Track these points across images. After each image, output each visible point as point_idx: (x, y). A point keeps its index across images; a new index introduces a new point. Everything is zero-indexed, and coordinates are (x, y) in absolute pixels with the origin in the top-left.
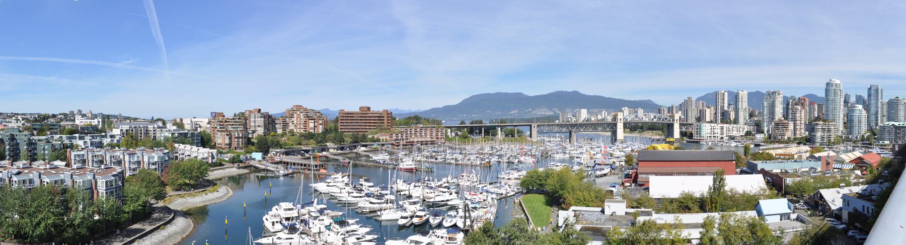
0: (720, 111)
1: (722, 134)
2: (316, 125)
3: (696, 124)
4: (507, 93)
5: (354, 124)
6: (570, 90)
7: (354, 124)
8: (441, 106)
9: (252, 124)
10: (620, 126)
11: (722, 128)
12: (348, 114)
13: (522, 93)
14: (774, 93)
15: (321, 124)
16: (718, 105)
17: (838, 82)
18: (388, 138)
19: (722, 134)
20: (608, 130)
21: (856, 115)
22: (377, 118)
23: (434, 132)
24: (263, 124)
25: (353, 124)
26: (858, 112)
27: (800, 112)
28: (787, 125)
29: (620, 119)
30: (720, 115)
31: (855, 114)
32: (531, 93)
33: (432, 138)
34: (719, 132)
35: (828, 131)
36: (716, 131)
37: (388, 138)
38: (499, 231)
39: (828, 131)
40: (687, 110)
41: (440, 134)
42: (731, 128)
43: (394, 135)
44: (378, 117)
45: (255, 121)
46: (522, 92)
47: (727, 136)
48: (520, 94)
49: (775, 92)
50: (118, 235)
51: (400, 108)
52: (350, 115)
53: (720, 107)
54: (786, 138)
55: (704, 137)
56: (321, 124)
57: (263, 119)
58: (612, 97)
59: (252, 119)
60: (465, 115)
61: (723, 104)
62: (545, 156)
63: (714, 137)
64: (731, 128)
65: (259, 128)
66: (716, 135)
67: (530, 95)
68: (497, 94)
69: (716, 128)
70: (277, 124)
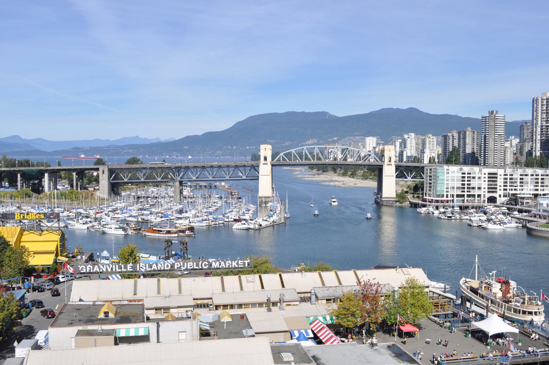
0: (539, 137)
1: (492, 189)
3: (428, 168)
4: (303, 113)
6: (404, 106)
8: (200, 134)
10: (389, 172)
11: (493, 177)
13: (327, 113)
16: (536, 124)
19: (492, 189)
27: (460, 146)
29: (265, 159)
30: (539, 145)
32: (340, 112)
34: (485, 185)
36: (475, 183)
38: (344, 355)
40: (485, 137)
42: (517, 176)
47: (504, 196)
48: (324, 114)
50: (517, 286)
51: (142, 136)
53: (539, 130)
55: (443, 196)
58: (459, 115)
60: (235, 147)
62: (317, 219)
63: (469, 196)
64: (517, 176)
66: (476, 192)
68: (288, 114)
69: (477, 176)
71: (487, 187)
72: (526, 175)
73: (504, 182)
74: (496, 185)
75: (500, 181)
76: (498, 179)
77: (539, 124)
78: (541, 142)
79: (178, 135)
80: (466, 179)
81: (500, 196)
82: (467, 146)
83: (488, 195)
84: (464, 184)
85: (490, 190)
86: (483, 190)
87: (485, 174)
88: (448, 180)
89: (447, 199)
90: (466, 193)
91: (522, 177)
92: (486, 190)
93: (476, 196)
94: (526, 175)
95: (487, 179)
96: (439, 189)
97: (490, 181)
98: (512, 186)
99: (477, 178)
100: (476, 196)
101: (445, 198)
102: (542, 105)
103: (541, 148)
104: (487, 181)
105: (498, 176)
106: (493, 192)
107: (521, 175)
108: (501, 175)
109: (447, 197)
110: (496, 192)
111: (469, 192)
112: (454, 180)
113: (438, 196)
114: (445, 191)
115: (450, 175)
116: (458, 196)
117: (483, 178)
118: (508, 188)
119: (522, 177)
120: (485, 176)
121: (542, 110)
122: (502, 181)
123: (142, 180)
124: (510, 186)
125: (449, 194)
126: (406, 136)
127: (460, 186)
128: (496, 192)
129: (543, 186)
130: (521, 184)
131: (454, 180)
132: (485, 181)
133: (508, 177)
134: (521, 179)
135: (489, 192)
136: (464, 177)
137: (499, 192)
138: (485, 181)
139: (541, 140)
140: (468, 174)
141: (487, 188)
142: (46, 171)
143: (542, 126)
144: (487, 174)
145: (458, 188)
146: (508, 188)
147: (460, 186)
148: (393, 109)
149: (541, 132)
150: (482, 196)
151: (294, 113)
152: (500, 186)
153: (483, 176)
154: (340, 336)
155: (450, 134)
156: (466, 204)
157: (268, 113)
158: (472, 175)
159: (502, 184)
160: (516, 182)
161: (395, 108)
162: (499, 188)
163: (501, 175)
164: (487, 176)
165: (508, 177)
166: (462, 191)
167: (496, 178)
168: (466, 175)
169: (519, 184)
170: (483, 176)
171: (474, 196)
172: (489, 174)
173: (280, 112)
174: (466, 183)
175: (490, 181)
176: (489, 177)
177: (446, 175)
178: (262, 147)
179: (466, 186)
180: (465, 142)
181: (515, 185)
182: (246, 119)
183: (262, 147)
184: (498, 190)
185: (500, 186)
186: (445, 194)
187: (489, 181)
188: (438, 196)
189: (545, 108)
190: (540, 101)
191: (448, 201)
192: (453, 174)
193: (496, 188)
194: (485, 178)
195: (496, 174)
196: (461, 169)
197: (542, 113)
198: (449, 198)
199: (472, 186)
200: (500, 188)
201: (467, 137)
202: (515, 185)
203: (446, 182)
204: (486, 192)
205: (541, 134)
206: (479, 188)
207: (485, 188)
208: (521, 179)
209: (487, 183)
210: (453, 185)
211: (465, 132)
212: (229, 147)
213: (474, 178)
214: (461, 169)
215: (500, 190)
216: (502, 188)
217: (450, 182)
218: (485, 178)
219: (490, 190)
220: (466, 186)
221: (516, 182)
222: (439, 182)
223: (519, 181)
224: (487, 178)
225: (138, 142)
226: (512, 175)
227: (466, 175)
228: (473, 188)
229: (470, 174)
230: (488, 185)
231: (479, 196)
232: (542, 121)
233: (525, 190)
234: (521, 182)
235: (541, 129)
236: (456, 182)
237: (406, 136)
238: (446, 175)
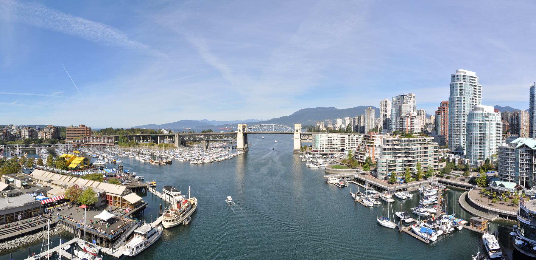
1: (343, 145)
2: (46, 135)
4: (324, 108)
5: (76, 134)
7: (76, 134)
8: (279, 117)
9: (23, 134)
11: (343, 139)
12: (73, 129)
14: (402, 97)
15: (49, 135)
17: (469, 73)
18: (72, 142)
19: (343, 145)
20: (192, 140)
21: (475, 124)
22: (81, 131)
23: (106, 139)
24: (28, 134)
25: (73, 134)
26: (480, 118)
28: (373, 140)
31: (474, 122)
33: (105, 143)
34: (339, 143)
35: (406, 153)
36: (334, 142)
37: (72, 142)
39: (406, 153)
41: (102, 140)
43: (76, 140)
44: (82, 130)
45: (24, 133)
46: (334, 107)
48: (333, 108)
49: (403, 96)
51: (255, 119)
52: (71, 130)
53: (382, 116)
54: (365, 158)
56: (49, 135)
57: (28, 132)
59: (23, 132)
61: (386, 112)
63: (331, 148)
64: (355, 138)
65: (26, 136)
66: (335, 147)
67: (340, 108)
68: (317, 108)
69: (335, 138)
70: (39, 134)
71: (340, 144)
72: (359, 138)
73: (349, 142)
74: (345, 143)
75: (347, 141)
76: (346, 140)
77: (382, 113)
78: (383, 122)
79: (270, 118)
80: (330, 140)
81: (347, 148)
82: (361, 123)
83: (341, 148)
84: (329, 143)
85: (342, 145)
86: (338, 145)
87: (339, 138)
88: (321, 141)
89: (321, 150)
90: (330, 147)
91: (357, 139)
92: (340, 145)
93: (335, 148)
94: (359, 138)
95: (340, 140)
96: (316, 145)
97: (342, 141)
98: (353, 143)
99: (335, 140)
100: (335, 148)
101: (320, 150)
102: (383, 104)
103: (383, 124)
104: (340, 141)
105: (346, 138)
106: (343, 146)
107: (357, 138)
108: (347, 138)
109: (321, 149)
110: (345, 146)
111: (332, 146)
112: (324, 141)
113: (317, 149)
114: (320, 146)
115: (322, 138)
116: (326, 148)
117: (338, 139)
118: (351, 144)
119: (357, 139)
120: (339, 138)
121: (383, 107)
122: (348, 141)
123: (211, 139)
124: (351, 143)
125: (322, 148)
126: (345, 118)
127: (327, 143)
128: (345, 146)
129: (332, 145)
130: (357, 142)
131: (324, 141)
132: (339, 141)
133: (351, 139)
134: (357, 140)
135: (341, 146)
136: (329, 139)
137: (346, 146)
138: (339, 141)
139: (383, 120)
140: (331, 137)
141: (340, 145)
142: (134, 136)
143: (383, 114)
144: (340, 138)
145: (326, 145)
146: (351, 144)
147: (327, 143)
148: (363, 106)
149: (383, 117)
150: (338, 148)
151: (320, 108)
152: (347, 143)
153: (338, 138)
154: (46, 250)
155: (356, 118)
156: (325, 152)
157: (345, 108)
158: (333, 138)
159: (348, 143)
160: (354, 141)
161: (364, 106)
162: (346, 144)
163: (347, 138)
164: (340, 138)
165: (351, 139)
166: (328, 146)
167: (345, 139)
168: (330, 138)
169: (356, 142)
170: (338, 138)
171: (334, 148)
172: (341, 137)
173: (314, 107)
174: (330, 142)
175: (342, 141)
176: (341, 139)
177: (320, 138)
178: (296, 125)
179: (330, 144)
180: (360, 121)
181: (354, 143)
182: (299, 111)
183: (296, 125)
184: (346, 145)
185: (347, 143)
186: (320, 147)
187: (341, 141)
188: (317, 149)
189: (384, 106)
190: (382, 103)
191: (321, 151)
192: (323, 138)
193: (345, 144)
194: (339, 139)
195: (345, 137)
196: (327, 135)
197: (383, 108)
198: (322, 150)
199: (333, 143)
200: (347, 144)
201: (361, 119)
202: (354, 143)
203: (320, 142)
204: (340, 146)
205: (383, 118)
206: (337, 145)
207: (339, 145)
208: (357, 140)
209: (340, 142)
210: (323, 143)
211: (360, 117)
212: (291, 123)
213: (334, 139)
214: (327, 135)
215: (347, 145)
216: (348, 144)
217: (322, 142)
218: (339, 139)
219: (342, 145)
220: (330, 144)
221: (354, 141)
222: (317, 141)
223: (356, 141)
224: (340, 139)
225: (254, 121)
226: (352, 138)
227: (330, 138)
228: (334, 145)
229: (332, 137)
230: (341, 143)
231: (336, 148)
232: (383, 112)
233: (271, 149)
234: (357, 141)
235: (383, 115)
236: (325, 142)
237: (345, 118)
238: (320, 138)
